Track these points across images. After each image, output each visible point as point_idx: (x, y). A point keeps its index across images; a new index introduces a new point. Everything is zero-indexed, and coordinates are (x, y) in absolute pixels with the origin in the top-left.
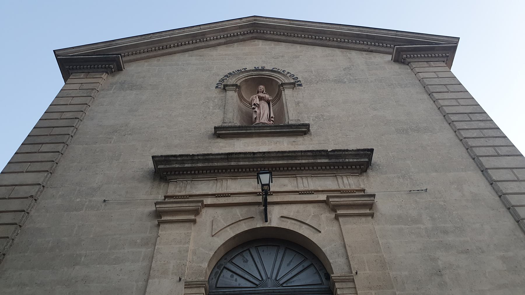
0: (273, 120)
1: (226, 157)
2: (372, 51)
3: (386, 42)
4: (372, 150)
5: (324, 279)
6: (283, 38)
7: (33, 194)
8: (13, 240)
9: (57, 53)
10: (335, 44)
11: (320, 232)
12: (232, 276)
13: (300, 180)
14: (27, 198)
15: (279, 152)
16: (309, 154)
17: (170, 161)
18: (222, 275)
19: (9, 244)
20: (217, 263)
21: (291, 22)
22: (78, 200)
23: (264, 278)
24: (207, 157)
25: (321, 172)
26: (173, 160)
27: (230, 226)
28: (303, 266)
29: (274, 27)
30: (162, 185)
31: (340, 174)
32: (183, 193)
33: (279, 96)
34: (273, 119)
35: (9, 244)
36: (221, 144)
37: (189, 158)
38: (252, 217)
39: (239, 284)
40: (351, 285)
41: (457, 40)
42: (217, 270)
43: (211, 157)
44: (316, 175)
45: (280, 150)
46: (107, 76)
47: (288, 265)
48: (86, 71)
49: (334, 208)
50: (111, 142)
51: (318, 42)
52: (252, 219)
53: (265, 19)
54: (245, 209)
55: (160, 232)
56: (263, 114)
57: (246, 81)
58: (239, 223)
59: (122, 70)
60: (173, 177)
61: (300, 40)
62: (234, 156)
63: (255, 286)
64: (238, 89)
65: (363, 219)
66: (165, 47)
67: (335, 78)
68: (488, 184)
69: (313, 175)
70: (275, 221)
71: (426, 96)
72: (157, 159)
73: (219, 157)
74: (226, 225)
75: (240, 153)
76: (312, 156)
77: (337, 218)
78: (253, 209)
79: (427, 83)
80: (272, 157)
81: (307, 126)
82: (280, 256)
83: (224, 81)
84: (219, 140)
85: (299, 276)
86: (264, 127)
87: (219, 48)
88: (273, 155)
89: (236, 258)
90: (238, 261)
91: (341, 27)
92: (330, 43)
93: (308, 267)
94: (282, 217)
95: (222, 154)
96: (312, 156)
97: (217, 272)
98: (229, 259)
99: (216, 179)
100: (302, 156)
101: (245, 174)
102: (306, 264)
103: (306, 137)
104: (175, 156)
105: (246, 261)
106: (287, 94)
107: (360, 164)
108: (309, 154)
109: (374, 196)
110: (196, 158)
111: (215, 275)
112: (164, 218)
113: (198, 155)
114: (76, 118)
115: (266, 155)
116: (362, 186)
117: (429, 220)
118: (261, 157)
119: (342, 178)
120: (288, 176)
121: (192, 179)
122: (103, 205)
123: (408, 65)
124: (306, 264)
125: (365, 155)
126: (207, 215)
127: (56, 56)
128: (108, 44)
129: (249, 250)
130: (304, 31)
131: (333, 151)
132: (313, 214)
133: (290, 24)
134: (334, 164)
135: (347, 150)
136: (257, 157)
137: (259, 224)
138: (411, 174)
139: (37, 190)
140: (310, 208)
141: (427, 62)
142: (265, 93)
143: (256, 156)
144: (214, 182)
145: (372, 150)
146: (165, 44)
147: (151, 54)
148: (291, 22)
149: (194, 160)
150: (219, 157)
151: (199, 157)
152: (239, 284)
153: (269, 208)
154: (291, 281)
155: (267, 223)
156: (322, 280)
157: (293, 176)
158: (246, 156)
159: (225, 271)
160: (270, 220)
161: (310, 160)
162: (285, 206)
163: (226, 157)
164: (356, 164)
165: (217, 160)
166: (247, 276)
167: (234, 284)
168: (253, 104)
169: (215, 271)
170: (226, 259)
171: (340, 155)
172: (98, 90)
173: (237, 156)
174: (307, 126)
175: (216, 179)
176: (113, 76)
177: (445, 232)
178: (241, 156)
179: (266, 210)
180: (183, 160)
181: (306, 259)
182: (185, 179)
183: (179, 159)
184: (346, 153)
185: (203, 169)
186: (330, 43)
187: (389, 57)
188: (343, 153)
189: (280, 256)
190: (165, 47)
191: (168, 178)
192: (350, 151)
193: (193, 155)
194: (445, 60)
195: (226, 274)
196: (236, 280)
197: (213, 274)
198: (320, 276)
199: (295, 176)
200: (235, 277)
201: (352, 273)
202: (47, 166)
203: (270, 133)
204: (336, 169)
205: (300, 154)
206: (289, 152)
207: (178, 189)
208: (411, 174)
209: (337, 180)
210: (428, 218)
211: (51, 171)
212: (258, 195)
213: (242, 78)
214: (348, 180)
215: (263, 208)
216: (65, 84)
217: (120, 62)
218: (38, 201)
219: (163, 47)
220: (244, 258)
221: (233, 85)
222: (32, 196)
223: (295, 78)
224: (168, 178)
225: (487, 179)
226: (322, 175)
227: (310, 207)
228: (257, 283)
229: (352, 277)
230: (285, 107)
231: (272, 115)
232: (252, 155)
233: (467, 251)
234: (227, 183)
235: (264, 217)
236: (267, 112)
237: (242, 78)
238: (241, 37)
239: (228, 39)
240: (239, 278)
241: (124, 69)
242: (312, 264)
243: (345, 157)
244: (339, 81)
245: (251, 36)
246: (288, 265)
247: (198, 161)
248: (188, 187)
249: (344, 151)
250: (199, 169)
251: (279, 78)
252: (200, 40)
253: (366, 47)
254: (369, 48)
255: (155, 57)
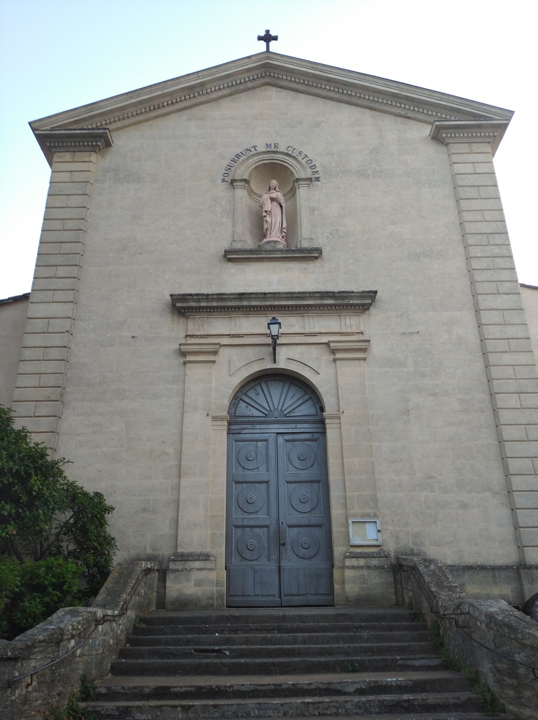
0: (285, 232)
1: (239, 296)
2: (409, 118)
3: (428, 107)
4: (375, 292)
5: (319, 411)
6: (303, 88)
7: (68, 329)
8: (66, 374)
9: (32, 126)
10: (367, 103)
11: (319, 374)
12: (247, 407)
13: (306, 318)
14: (64, 333)
15: (288, 293)
16: (317, 295)
17: (187, 299)
18: (239, 406)
19: (65, 379)
20: (235, 395)
21: (314, 66)
22: (109, 335)
23: (272, 409)
24: (221, 297)
25: (327, 311)
26: (190, 299)
27: (245, 366)
28: (303, 399)
29: (292, 72)
30: (182, 320)
31: (344, 314)
32: (202, 333)
33: (292, 193)
34: (285, 231)
35: (65, 379)
36: (233, 271)
37: (204, 297)
38: (263, 359)
39: (253, 414)
40: (337, 421)
41: (510, 115)
42: (234, 401)
43: (225, 296)
44: (322, 315)
45: (290, 291)
46: (96, 158)
47: (292, 398)
48: (71, 149)
49: (333, 352)
50: (123, 264)
51: (345, 98)
52: (263, 360)
53: (280, 58)
54: (257, 349)
55: (187, 372)
56: (275, 223)
57: (257, 167)
58: (252, 363)
59: (112, 146)
60: (191, 314)
61: (324, 93)
62: (246, 296)
63: (265, 415)
64: (247, 185)
65: (357, 362)
66: (156, 107)
67: (359, 168)
68: (476, 326)
69: (319, 315)
70: (282, 364)
71: (452, 203)
72: (175, 297)
73: (232, 296)
74: (241, 366)
75: (252, 294)
76: (320, 297)
77: (335, 360)
78: (264, 349)
79: (460, 183)
80: (283, 297)
81: (319, 251)
82: (285, 391)
83: (230, 169)
84: (230, 265)
85: (300, 408)
86: (275, 251)
87: (223, 102)
88: (283, 296)
89: (250, 392)
90: (251, 394)
91: (376, 80)
92: (360, 102)
93: (307, 400)
94: (288, 359)
95: (235, 294)
96: (320, 297)
97: (234, 403)
98: (244, 392)
99: (229, 316)
100: (310, 297)
101: (257, 313)
102: (306, 398)
103: (317, 263)
104: (191, 295)
105: (258, 394)
106: (302, 192)
107: (363, 305)
108: (317, 295)
109: (369, 341)
110: (211, 297)
111: (234, 405)
112: (189, 358)
113: (212, 295)
114: (80, 230)
115: (277, 296)
116: (362, 329)
117: (413, 363)
118: (272, 297)
119: (345, 318)
120: (296, 315)
121: (207, 316)
122: (132, 340)
123: (446, 145)
124: (306, 398)
125: (369, 296)
126: (224, 354)
127: (34, 130)
128: (90, 108)
129: (260, 384)
130: (329, 80)
131: (340, 292)
132: (315, 357)
133: (313, 68)
134: (339, 305)
135: (353, 292)
136: (267, 298)
137: (269, 365)
138: (409, 313)
139: (70, 325)
140: (314, 350)
141: (469, 143)
142: (278, 190)
143: (267, 296)
144: (228, 320)
145: (375, 292)
146: (156, 102)
147: (142, 117)
148: (314, 66)
149: (209, 299)
150: (232, 296)
151: (214, 296)
152: (253, 414)
153: (278, 349)
154: (295, 411)
155: (276, 364)
156: (317, 412)
157: (301, 315)
158: (257, 296)
159: (241, 402)
160: (278, 362)
161: (317, 301)
162: (291, 347)
163: (239, 296)
164: (359, 305)
165: (231, 300)
166: (258, 407)
167: (249, 413)
168: (264, 211)
169: (233, 402)
170: (241, 392)
171: (346, 296)
172: (92, 182)
173: (249, 296)
174: (319, 251)
175: (229, 316)
176: (103, 156)
177: (423, 376)
178: (253, 296)
179: (274, 349)
180: (199, 299)
181: (306, 393)
182: (202, 316)
183: (195, 297)
184: (352, 294)
185: (217, 307)
186: (360, 102)
187: (427, 130)
188: (349, 294)
189: (285, 391)
190: (156, 107)
191: (186, 314)
192: (356, 293)
193: (208, 295)
194: (492, 141)
195: (242, 405)
196: (250, 410)
197: (232, 405)
198: (316, 407)
199: (302, 315)
200: (250, 407)
201: (339, 412)
202: (70, 296)
203: (282, 258)
204: (341, 309)
205: (308, 295)
206: (299, 293)
207: (197, 327)
208: (409, 313)
209: (340, 321)
210: (412, 362)
211: (76, 302)
212: (268, 336)
213: (252, 165)
214: (350, 320)
215: (271, 349)
216: (50, 170)
217: (109, 138)
218: (74, 335)
219: (154, 106)
220: (257, 391)
221: (242, 180)
222: (68, 331)
223: (312, 166)
224: (186, 314)
225: (477, 321)
226: (327, 315)
227: (313, 349)
228: (267, 413)
229: (339, 415)
230: (299, 217)
231: (285, 225)
232: (263, 296)
233: (434, 394)
234: (240, 322)
235: (273, 358)
236: (279, 219)
237: (252, 165)
238: (250, 85)
239: (234, 89)
240: (252, 409)
241: (113, 143)
242: (311, 398)
243: (351, 298)
244: (362, 174)
245: (262, 81)
246: (292, 398)
247: (212, 300)
248: (206, 325)
249: (350, 292)
250: (213, 308)
251: (294, 166)
252: (199, 93)
253: (403, 113)
254: (406, 114)
255: (146, 120)
